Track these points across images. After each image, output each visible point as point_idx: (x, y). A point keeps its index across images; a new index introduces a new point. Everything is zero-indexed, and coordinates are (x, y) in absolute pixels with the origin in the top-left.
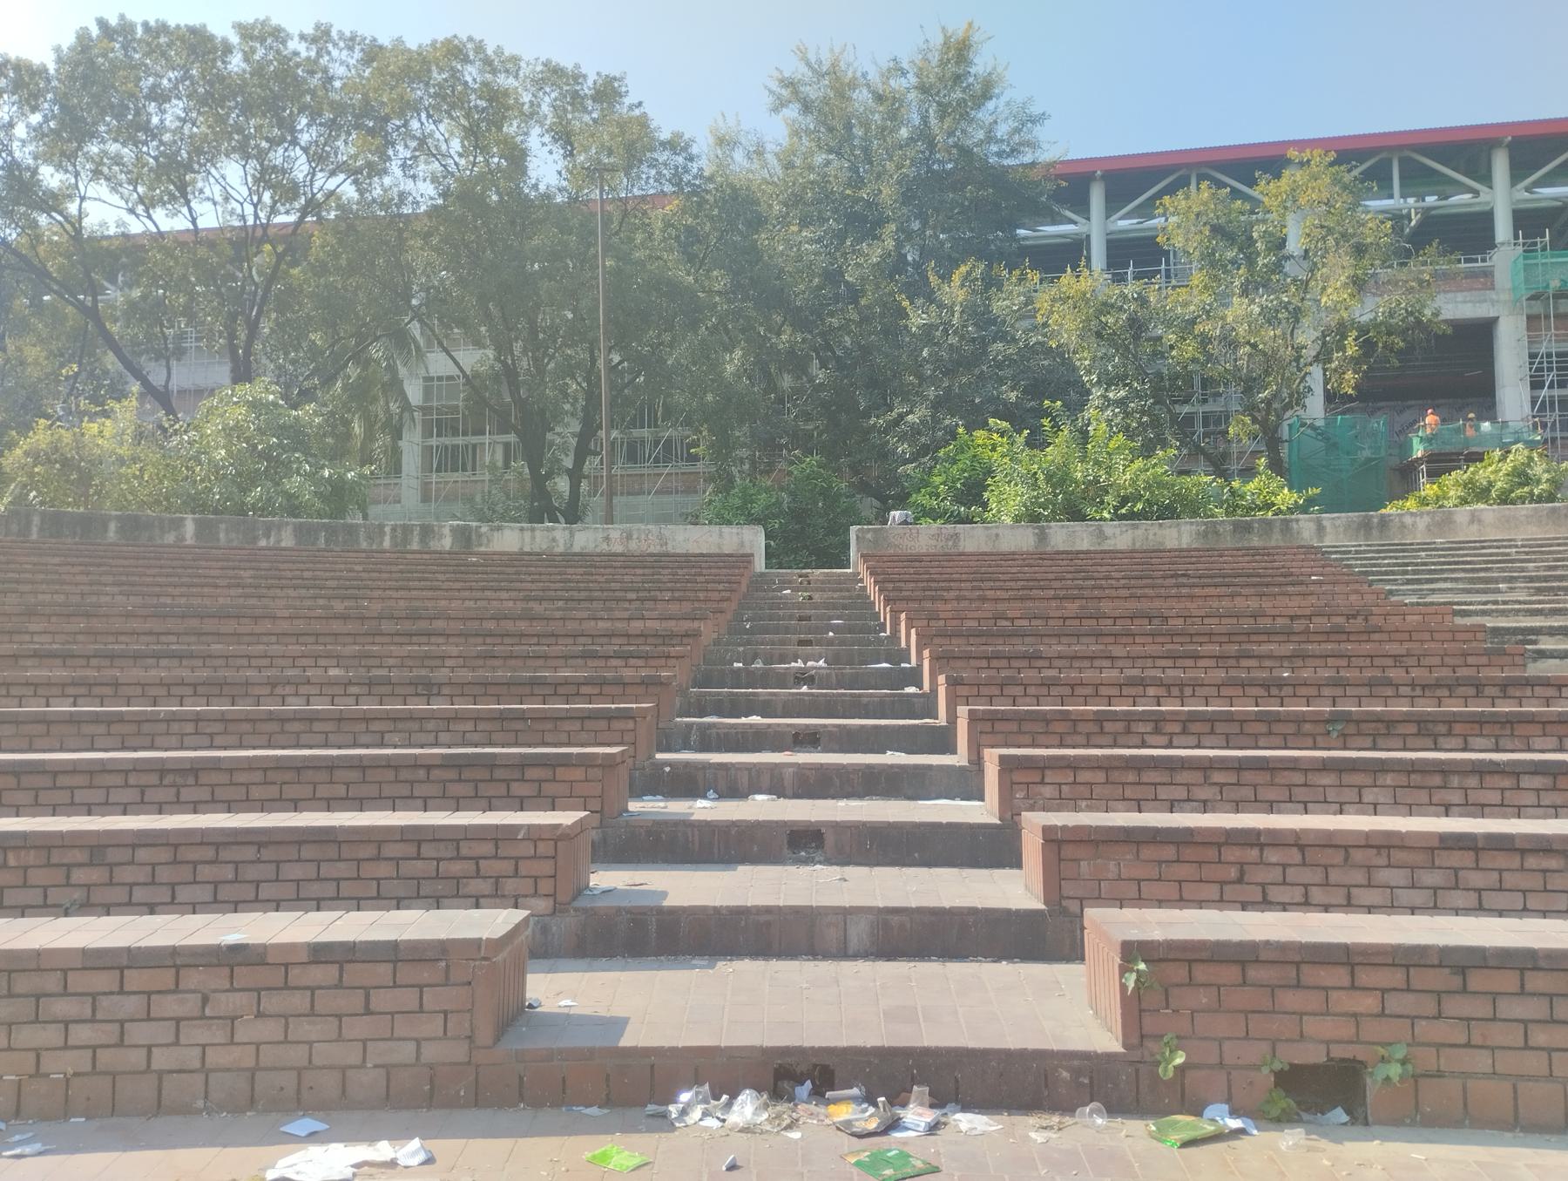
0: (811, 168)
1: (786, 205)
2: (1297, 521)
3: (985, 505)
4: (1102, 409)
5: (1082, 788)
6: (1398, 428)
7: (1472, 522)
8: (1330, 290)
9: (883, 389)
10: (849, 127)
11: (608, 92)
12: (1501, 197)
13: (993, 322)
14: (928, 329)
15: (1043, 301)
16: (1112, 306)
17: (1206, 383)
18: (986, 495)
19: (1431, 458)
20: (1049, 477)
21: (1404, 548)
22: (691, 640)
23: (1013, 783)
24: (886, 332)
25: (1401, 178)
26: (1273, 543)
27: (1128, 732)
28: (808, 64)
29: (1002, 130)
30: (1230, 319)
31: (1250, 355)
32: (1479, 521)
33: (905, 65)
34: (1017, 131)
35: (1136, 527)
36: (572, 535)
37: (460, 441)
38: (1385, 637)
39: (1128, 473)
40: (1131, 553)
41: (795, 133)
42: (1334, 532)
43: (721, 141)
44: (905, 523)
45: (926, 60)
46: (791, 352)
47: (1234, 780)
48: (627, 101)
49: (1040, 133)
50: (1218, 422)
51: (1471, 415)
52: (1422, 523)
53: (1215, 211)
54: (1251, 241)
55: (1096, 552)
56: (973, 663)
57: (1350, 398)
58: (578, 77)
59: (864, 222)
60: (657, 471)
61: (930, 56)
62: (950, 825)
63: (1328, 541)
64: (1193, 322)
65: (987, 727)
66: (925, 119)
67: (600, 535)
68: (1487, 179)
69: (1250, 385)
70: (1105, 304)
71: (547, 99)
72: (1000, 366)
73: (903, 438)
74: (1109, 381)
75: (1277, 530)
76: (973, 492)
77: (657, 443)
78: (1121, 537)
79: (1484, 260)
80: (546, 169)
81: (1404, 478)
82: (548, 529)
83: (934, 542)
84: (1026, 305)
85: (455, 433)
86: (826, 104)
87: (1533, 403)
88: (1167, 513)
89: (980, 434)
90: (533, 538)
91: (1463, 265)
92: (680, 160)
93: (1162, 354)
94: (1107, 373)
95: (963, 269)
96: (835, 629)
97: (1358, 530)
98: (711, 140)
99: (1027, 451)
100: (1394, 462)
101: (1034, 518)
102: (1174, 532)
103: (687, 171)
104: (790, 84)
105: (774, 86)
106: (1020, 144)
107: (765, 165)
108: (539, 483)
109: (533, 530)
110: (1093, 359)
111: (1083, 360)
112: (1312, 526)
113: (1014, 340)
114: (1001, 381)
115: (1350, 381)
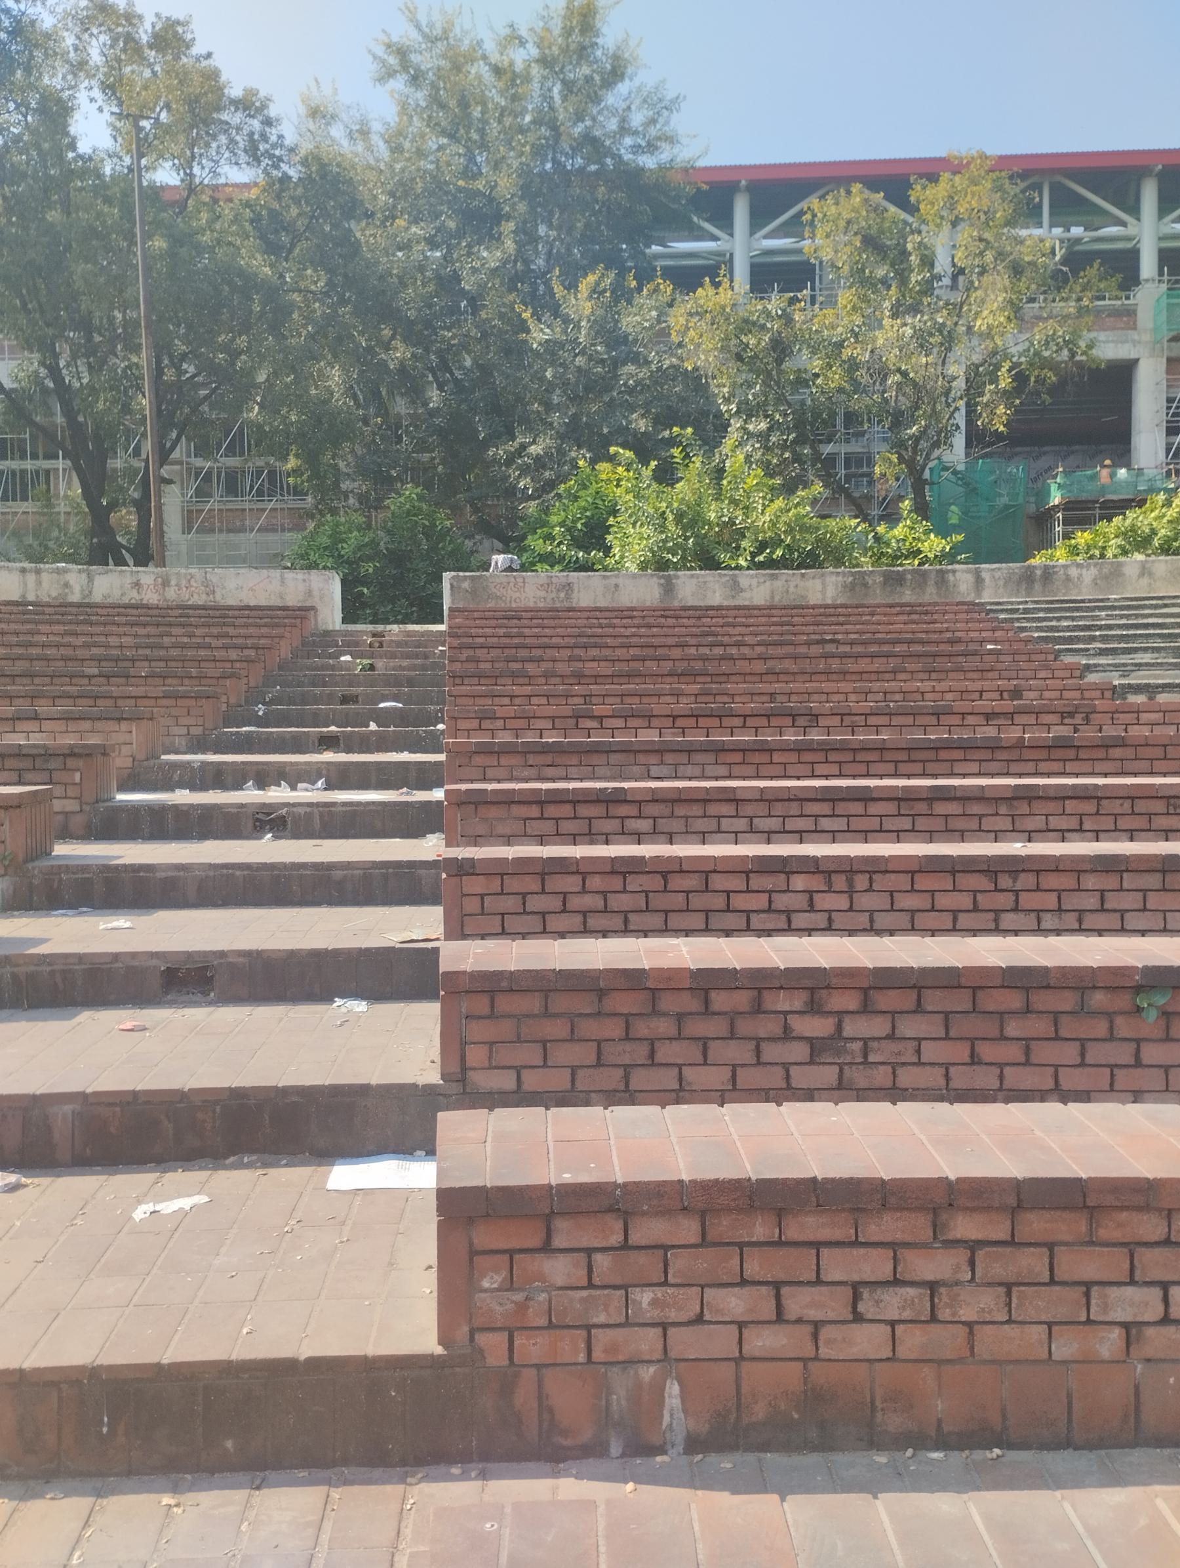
0: (420, 153)
1: (392, 194)
2: (954, 571)
3: (607, 550)
4: (740, 444)
5: (642, 1258)
6: (1033, 475)
7: (1142, 575)
8: (985, 313)
9: (507, 417)
10: (464, 104)
11: (170, 38)
12: (1147, 231)
13: (624, 340)
14: (552, 347)
15: (677, 319)
16: (754, 324)
17: (851, 418)
18: (609, 538)
19: (1067, 506)
20: (679, 517)
21: (1076, 606)
22: (80, 763)
23: (473, 1253)
24: (508, 352)
25: (1051, 206)
26: (926, 598)
27: (758, 1009)
28: (418, 27)
29: (637, 119)
30: (880, 342)
31: (899, 384)
32: (1150, 574)
33: (524, 33)
34: (653, 121)
35: (774, 577)
36: (90, 579)
37: (29, 465)
38: (1129, 753)
39: (768, 514)
40: (769, 609)
41: (404, 107)
42: (990, 585)
43: (315, 113)
44: (510, 569)
45: (548, 30)
46: (402, 369)
47: (1002, 1234)
48: (196, 50)
49: (679, 122)
50: (859, 464)
51: (1108, 462)
52: (1089, 574)
53: (867, 219)
54: (905, 254)
55: (728, 608)
56: (516, 810)
57: (998, 436)
58: (131, 18)
59: (482, 219)
60: (260, 505)
61: (551, 24)
62: (316, 1364)
63: (986, 597)
64: (840, 345)
65: (481, 1005)
66: (547, 97)
67: (128, 580)
68: (1135, 210)
69: (899, 420)
70: (746, 321)
71: (94, 42)
72: (631, 391)
73: (525, 470)
74: (748, 411)
75: (931, 582)
76: (593, 535)
77: (259, 473)
78: (758, 589)
79: (1128, 298)
80: (93, 129)
81: (1040, 527)
82: (58, 571)
83: (543, 594)
84: (659, 322)
85: (23, 457)
86: (445, 85)
87: (1168, 451)
88: (810, 561)
89: (603, 466)
90: (39, 583)
91: (1107, 302)
92: (256, 124)
93: (806, 381)
94: (747, 402)
95: (591, 278)
96: (383, 718)
97: (1019, 583)
98: (302, 110)
99: (655, 486)
100: (1032, 508)
101: (662, 566)
102: (817, 584)
103: (264, 137)
104: (402, 53)
105: (380, 51)
106: (659, 138)
107: (370, 148)
108: (100, 518)
109: (38, 572)
110: (734, 385)
111: (721, 388)
112: (970, 578)
113: (647, 362)
114: (632, 408)
115: (999, 418)
